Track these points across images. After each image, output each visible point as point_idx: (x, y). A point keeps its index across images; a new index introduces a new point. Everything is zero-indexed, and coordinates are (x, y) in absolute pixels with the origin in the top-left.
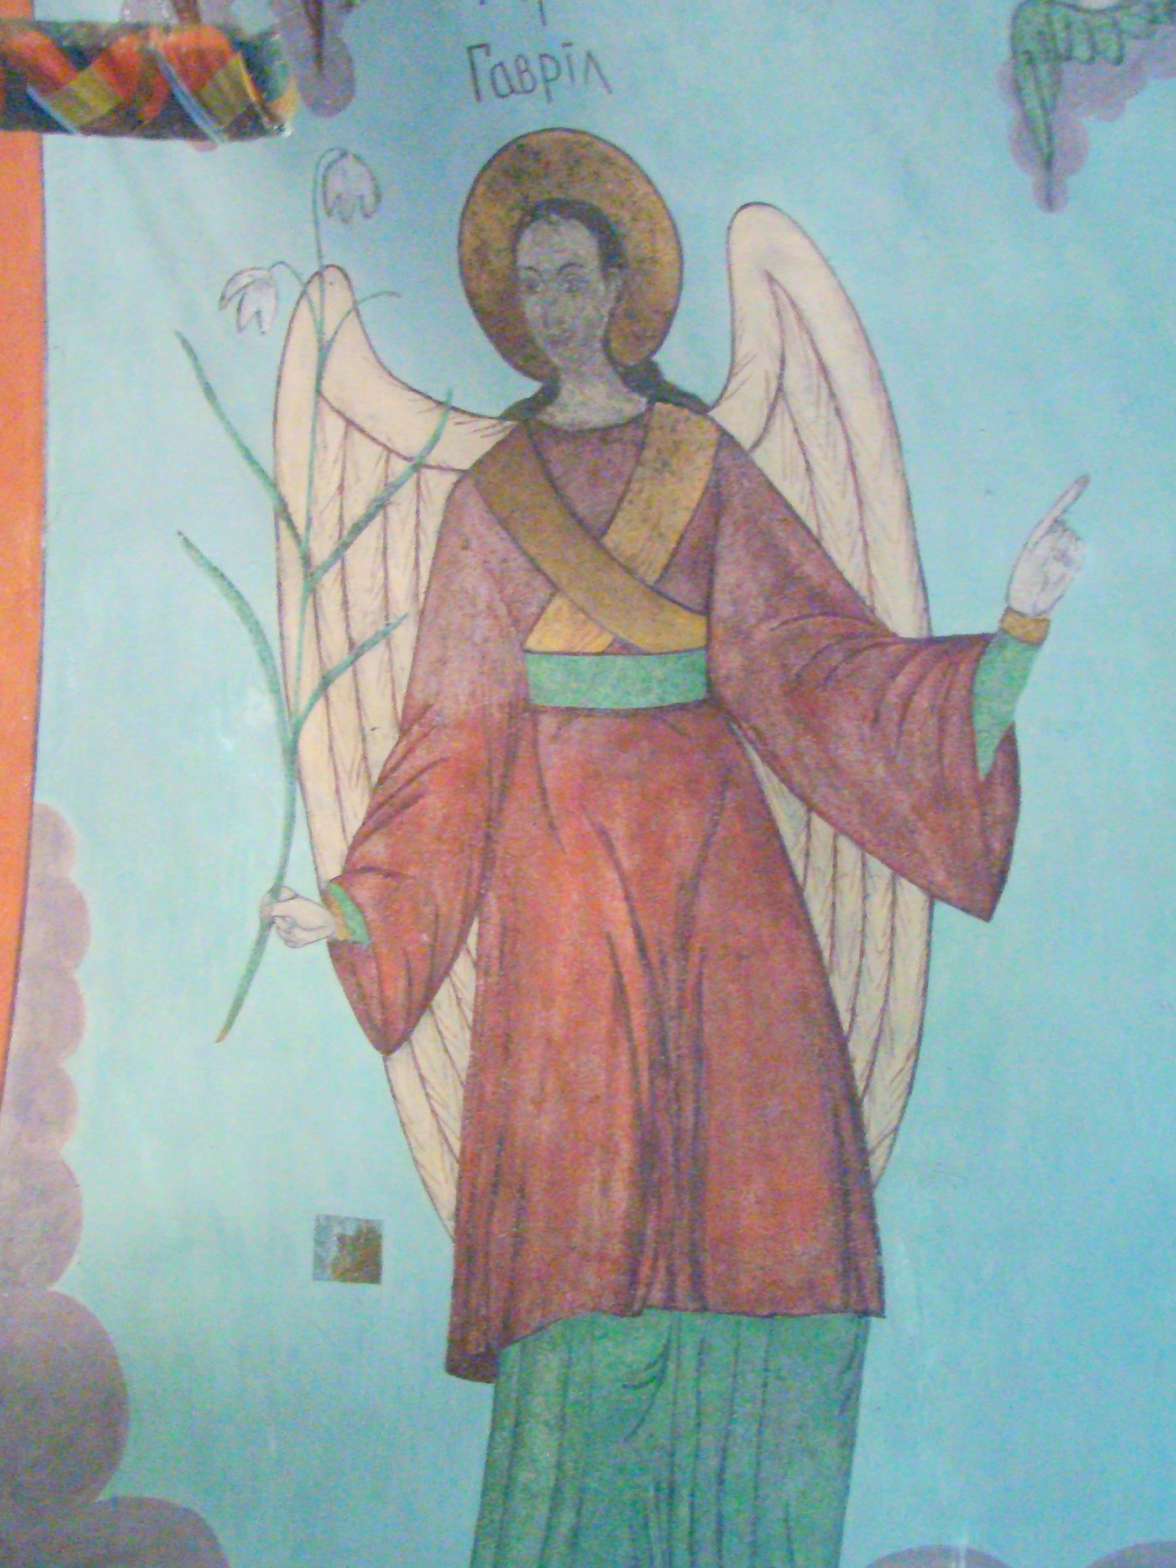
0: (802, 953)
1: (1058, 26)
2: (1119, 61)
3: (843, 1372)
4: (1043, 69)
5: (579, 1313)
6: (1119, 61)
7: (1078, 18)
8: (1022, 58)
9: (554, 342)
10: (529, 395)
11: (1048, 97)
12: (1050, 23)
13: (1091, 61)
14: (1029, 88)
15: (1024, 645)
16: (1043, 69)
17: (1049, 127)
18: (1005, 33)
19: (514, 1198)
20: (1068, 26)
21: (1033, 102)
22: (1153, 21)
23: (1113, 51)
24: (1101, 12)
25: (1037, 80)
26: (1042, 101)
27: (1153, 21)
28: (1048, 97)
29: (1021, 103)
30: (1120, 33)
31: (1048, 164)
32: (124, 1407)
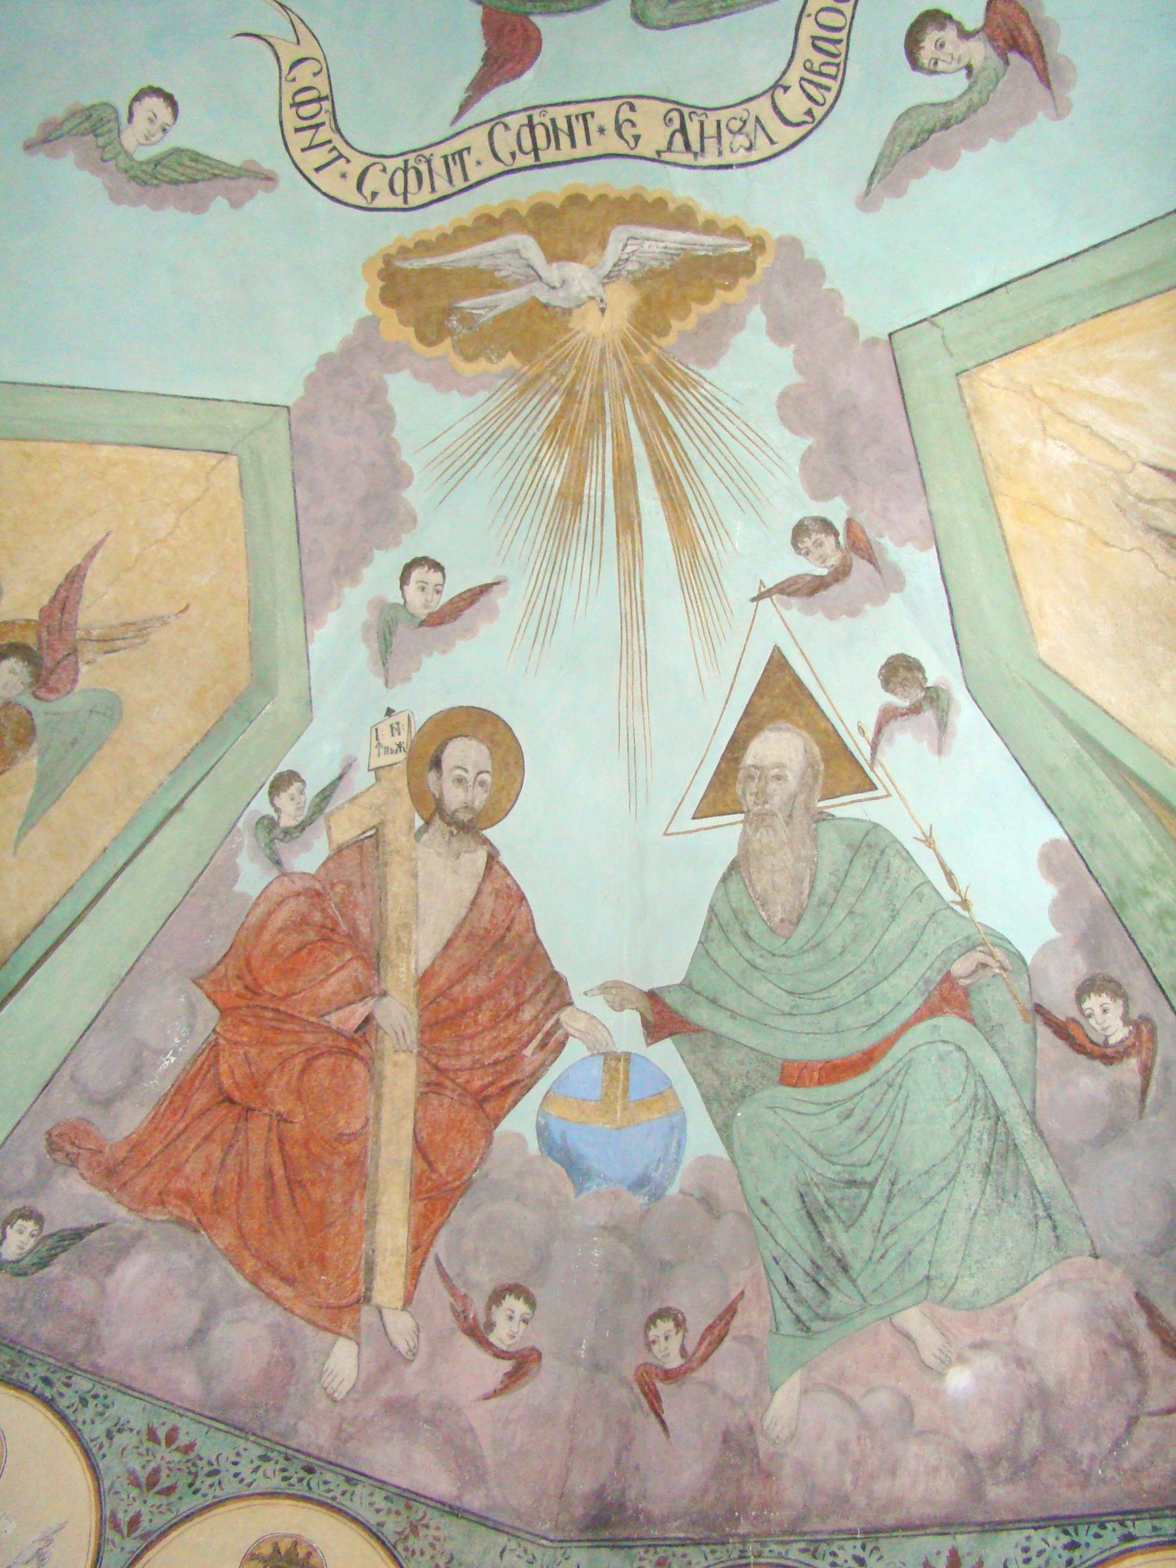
0: (791, 1076)
1: (108, 126)
2: (103, 160)
3: (907, 1097)
4: (87, 125)
5: (245, 949)
6: (103, 160)
7: (114, 134)
8: (87, 113)
9: (92, 1440)
10: (763, 320)
11: (74, 132)
12: (109, 121)
13: (98, 147)
14: (76, 121)
15: (831, 1315)
16: (87, 125)
17: (61, 136)
18: (96, 101)
19: (365, 951)
20: (110, 131)
21: (68, 126)
22: (126, 171)
23: (107, 156)
24: (122, 146)
25: (80, 124)
26: (72, 129)
27: (126, 171)
28: (74, 132)
29: (67, 119)
30: (115, 158)
31: (46, 141)
32: (284, 1546)
